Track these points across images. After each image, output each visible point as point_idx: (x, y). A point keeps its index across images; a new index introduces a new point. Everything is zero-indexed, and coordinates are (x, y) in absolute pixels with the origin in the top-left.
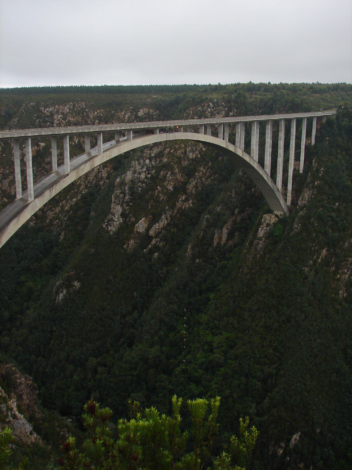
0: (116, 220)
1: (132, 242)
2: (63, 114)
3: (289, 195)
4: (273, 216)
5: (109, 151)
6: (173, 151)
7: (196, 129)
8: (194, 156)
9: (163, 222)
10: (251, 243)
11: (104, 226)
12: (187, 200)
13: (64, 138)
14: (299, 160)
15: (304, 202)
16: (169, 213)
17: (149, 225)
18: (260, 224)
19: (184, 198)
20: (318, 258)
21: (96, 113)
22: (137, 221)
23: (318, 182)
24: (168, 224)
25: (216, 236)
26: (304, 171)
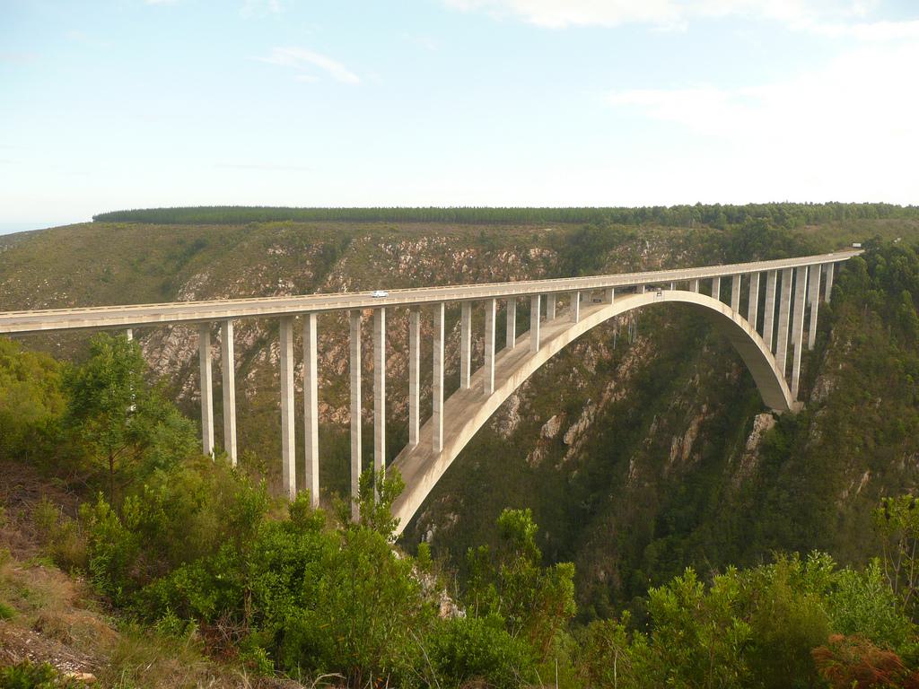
0: (512, 418)
1: (538, 452)
2: (412, 253)
3: (796, 384)
4: (770, 417)
7: (684, 286)
9: (581, 426)
10: (737, 460)
12: (617, 389)
15: (822, 396)
16: (592, 410)
17: (561, 427)
18: (751, 428)
19: (613, 385)
20: (856, 486)
22: (544, 421)
23: (844, 365)
24: (592, 426)
25: (674, 446)
26: (815, 346)
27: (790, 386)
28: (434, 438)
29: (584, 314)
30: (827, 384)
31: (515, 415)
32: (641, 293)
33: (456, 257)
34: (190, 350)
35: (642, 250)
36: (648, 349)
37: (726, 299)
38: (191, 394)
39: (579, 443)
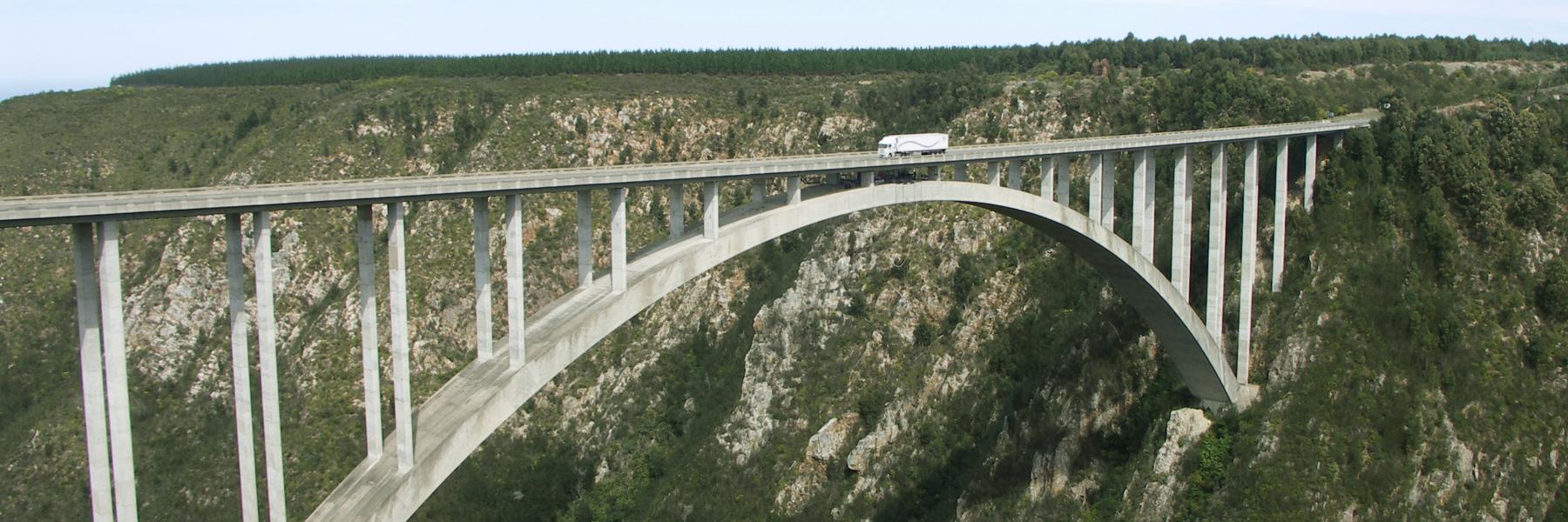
0: (755, 423)
1: (800, 485)
2: (612, 129)
6: (917, 234)
8: (976, 245)
11: (722, 441)
12: (954, 369)
14: (1271, 257)
18: (1163, 435)
19: (945, 364)
34: (213, 308)
36: (1014, 296)
37: (1080, 200)
38: (210, 385)
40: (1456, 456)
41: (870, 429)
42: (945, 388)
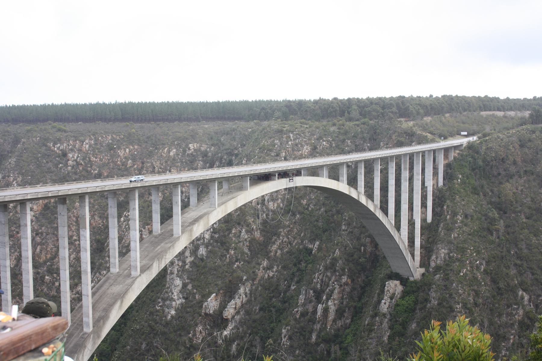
3: (417, 253)
5: (224, 205)
7: (314, 171)
8: (276, 205)
12: (269, 268)
13: (41, 184)
14: (426, 207)
17: (221, 304)
18: (382, 291)
21: (127, 150)
22: (205, 297)
27: (413, 255)
28: (84, 319)
29: (221, 201)
30: (443, 252)
31: (178, 295)
32: (274, 180)
33: (121, 153)
35: (287, 142)
37: (352, 182)
39: (237, 317)
40: (522, 298)
41: (231, 297)
42: (266, 276)
